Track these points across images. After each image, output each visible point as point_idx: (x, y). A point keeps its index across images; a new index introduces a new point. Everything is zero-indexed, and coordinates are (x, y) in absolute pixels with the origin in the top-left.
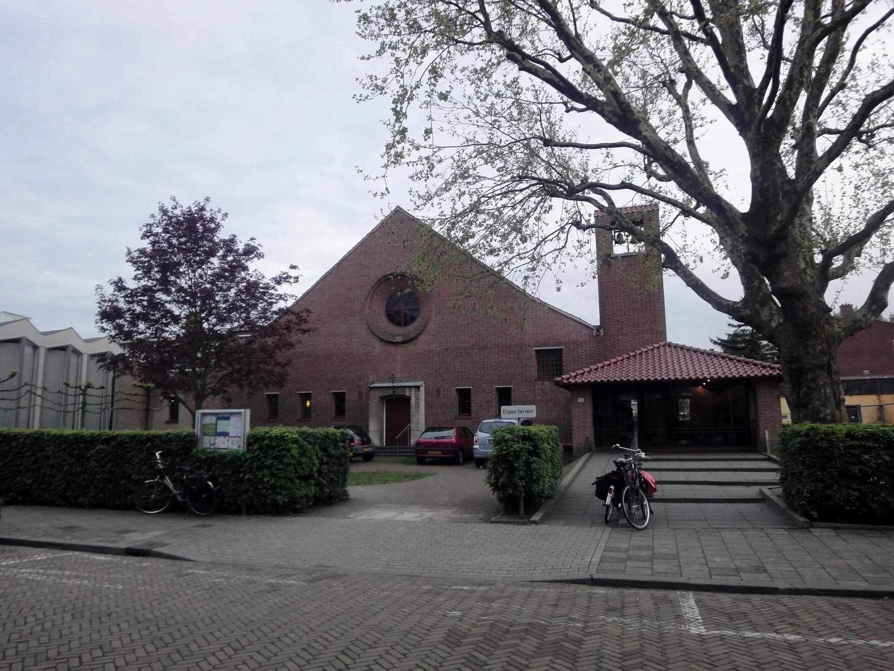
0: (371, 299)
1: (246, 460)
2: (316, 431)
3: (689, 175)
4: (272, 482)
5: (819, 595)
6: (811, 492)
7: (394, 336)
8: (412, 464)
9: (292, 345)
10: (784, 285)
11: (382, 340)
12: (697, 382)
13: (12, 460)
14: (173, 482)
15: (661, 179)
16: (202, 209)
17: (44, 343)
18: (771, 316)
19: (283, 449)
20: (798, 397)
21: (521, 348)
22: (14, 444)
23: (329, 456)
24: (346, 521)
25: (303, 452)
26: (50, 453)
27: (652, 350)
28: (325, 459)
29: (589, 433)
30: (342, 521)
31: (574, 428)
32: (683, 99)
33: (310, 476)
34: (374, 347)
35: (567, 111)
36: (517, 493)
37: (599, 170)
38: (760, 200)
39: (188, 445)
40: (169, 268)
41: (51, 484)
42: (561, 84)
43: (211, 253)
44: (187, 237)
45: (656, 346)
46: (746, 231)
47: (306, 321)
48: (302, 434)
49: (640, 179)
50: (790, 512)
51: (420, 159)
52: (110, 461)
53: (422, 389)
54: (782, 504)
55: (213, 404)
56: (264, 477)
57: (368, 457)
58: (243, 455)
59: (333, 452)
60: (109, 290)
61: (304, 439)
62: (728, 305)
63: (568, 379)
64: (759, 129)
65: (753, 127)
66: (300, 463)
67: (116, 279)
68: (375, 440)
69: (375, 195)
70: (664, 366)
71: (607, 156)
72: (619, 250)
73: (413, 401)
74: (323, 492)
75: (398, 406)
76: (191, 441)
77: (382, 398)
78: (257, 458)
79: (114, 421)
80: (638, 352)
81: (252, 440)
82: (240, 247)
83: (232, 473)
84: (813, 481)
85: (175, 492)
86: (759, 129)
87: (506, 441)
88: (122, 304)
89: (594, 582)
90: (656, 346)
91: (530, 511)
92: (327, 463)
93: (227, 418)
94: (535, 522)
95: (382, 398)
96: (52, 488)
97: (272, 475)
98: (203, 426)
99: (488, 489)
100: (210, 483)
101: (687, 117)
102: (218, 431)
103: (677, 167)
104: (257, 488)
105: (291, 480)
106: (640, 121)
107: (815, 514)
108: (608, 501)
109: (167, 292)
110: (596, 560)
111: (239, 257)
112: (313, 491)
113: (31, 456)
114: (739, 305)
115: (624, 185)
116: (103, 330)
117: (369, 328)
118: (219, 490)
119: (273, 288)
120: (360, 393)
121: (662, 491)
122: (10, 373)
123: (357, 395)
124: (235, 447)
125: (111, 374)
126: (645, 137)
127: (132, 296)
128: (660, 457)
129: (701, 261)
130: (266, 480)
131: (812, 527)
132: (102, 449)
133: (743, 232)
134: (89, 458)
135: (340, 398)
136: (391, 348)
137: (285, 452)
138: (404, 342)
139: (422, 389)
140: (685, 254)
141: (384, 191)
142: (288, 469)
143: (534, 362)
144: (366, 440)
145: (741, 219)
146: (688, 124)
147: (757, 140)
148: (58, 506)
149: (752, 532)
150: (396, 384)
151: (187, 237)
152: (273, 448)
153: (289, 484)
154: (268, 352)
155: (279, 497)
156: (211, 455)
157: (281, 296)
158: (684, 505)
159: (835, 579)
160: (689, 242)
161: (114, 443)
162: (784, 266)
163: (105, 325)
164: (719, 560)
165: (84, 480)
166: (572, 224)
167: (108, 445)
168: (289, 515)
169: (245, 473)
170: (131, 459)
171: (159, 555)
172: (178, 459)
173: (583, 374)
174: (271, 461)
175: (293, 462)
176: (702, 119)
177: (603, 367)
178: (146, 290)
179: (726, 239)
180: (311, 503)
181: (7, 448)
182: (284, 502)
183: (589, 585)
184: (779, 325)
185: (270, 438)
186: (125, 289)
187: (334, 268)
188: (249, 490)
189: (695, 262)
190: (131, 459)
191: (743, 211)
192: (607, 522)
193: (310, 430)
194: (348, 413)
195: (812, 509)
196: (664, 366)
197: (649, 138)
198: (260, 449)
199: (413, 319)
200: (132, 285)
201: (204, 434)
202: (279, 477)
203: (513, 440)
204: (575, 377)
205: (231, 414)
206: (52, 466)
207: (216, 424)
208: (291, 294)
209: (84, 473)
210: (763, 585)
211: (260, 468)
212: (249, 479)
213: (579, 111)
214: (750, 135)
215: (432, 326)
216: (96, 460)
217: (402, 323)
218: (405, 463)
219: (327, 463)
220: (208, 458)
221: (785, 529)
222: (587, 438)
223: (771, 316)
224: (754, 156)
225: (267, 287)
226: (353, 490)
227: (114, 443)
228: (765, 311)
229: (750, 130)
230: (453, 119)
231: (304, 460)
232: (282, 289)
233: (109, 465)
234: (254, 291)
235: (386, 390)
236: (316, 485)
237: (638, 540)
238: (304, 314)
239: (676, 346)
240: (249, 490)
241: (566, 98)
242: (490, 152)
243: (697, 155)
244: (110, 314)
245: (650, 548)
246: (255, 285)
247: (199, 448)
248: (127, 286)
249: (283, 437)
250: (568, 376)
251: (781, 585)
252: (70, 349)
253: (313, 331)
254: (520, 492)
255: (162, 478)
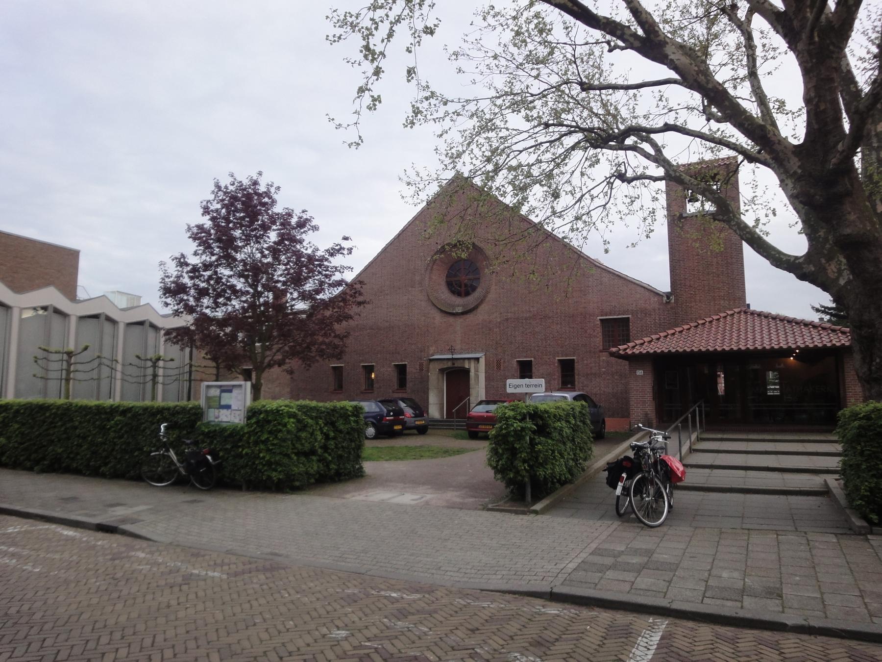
0: (432, 269)
1: (244, 434)
2: (321, 404)
3: (727, 103)
4: (268, 458)
5: (843, 637)
6: (871, 490)
7: (454, 306)
8: (463, 438)
9: (348, 317)
10: (848, 231)
11: (442, 311)
12: (789, 352)
13: (47, 430)
14: (176, 454)
15: (719, 121)
16: (255, 183)
17: (124, 319)
18: (840, 272)
19: (279, 424)
20: (870, 370)
21: (585, 317)
22: (47, 414)
23: (337, 430)
24: (344, 501)
25: (302, 427)
26: (77, 423)
27: (725, 317)
28: (332, 434)
29: (649, 408)
30: (337, 502)
31: (632, 403)
32: (745, 25)
33: (313, 452)
34: (434, 318)
35: (610, 51)
36: (519, 478)
37: (651, 117)
38: (816, 127)
39: (193, 418)
40: (228, 243)
41: (78, 454)
42: (575, 8)
43: (265, 228)
44: (243, 212)
45: (730, 312)
46: (799, 167)
47: (361, 294)
48: (301, 408)
49: (697, 122)
50: (848, 511)
51: (447, 113)
52: (126, 432)
53: (482, 361)
54: (843, 501)
55: (281, 375)
56: (260, 452)
57: (422, 431)
58: (242, 428)
59: (342, 427)
60: (173, 269)
61: (305, 413)
62: (788, 261)
63: (626, 349)
64: (811, 37)
65: (804, 36)
66: (299, 438)
67: (178, 255)
68: (434, 412)
69: (350, 146)
70: (735, 335)
71: (660, 100)
72: (692, 208)
73: (472, 374)
74: (329, 470)
75: (457, 378)
76: (195, 414)
77: (442, 371)
78: (253, 432)
79: (192, 390)
80: (708, 320)
81: (252, 413)
82: (294, 221)
83: (232, 447)
84: (874, 476)
85: (178, 465)
86: (811, 37)
87: (507, 419)
88: (186, 280)
89: (554, 597)
90: (730, 312)
91: (536, 499)
92: (334, 438)
93: (229, 391)
94: (536, 512)
95: (442, 371)
96: (79, 457)
97: (268, 450)
98: (208, 399)
99: (491, 473)
100: (209, 457)
101: (750, 46)
102: (222, 403)
103: (712, 94)
104: (254, 463)
105: (287, 456)
106: (667, 43)
107: (874, 517)
108: (619, 491)
109: (229, 266)
110: (572, 566)
111: (292, 229)
112: (315, 467)
113: (62, 426)
114: (801, 261)
115: (667, 128)
116: (167, 304)
117: (429, 299)
118: (220, 465)
119: (327, 260)
120: (421, 365)
121: (693, 477)
122: (83, 347)
123: (418, 367)
124: (237, 421)
125: (188, 350)
126: (672, 60)
127: (195, 271)
128: (725, 436)
129: (774, 214)
130: (261, 455)
131: (871, 533)
132: (119, 420)
133: (795, 168)
134: (109, 429)
135: (401, 370)
136: (451, 319)
137: (280, 427)
138: (464, 313)
139: (482, 361)
140: (755, 207)
141: (357, 140)
142: (283, 444)
143: (599, 330)
144: (420, 410)
145: (794, 153)
146: (751, 52)
147: (809, 52)
148: (84, 475)
149: (792, 537)
150: (455, 356)
151: (243, 212)
152: (269, 422)
153: (285, 461)
154: (325, 325)
155: (274, 474)
156: (213, 429)
157: (336, 268)
158: (728, 496)
159: (871, 616)
160: (759, 192)
161: (130, 415)
162: (847, 207)
163: (169, 300)
164: (729, 576)
165: (104, 450)
166: (617, 177)
167: (125, 416)
168: (287, 493)
169: (243, 447)
170: (144, 430)
171: (124, 533)
172: (185, 432)
173: (642, 344)
174: (265, 436)
175: (289, 437)
176: (774, 49)
177: (666, 337)
178: (207, 266)
179: (786, 182)
180: (313, 481)
181: (42, 418)
182: (279, 479)
183: (547, 599)
184: (849, 282)
185: (266, 411)
186: (187, 265)
187: (394, 239)
188: (247, 465)
189: (767, 216)
190: (144, 430)
191: (795, 142)
192: (619, 515)
193: (314, 403)
194: (409, 385)
195: (872, 511)
196: (735, 335)
197: (677, 62)
198: (257, 422)
199: (474, 289)
200: (194, 260)
201: (210, 407)
202: (274, 453)
203: (515, 418)
204: (633, 347)
205: (234, 386)
206: (79, 436)
207: (220, 397)
208: (351, 267)
209: (105, 443)
210: (767, 617)
211: (256, 443)
212: (247, 454)
213: (622, 49)
214: (800, 46)
215: (491, 296)
216: (115, 431)
217: (463, 294)
218: (456, 437)
219: (334, 438)
220: (209, 432)
221: (836, 534)
222: (646, 414)
223: (840, 272)
224: (807, 73)
225: (322, 259)
226: (368, 467)
227: (130, 415)
228: (833, 267)
229: (800, 39)
230: (484, 69)
231: (303, 435)
232: (336, 261)
233: (126, 436)
234: (308, 266)
235: (445, 362)
236: (319, 461)
237: (643, 540)
238: (358, 286)
239: (760, 314)
240: (247, 465)
241: (608, 37)
242: (520, 102)
243: (760, 87)
244: (174, 290)
245: (649, 553)
246: (311, 258)
247: (205, 421)
248: (189, 261)
249: (278, 411)
250: (625, 346)
251: (791, 618)
252: (147, 324)
253: (369, 303)
254: (523, 477)
255: (168, 451)
